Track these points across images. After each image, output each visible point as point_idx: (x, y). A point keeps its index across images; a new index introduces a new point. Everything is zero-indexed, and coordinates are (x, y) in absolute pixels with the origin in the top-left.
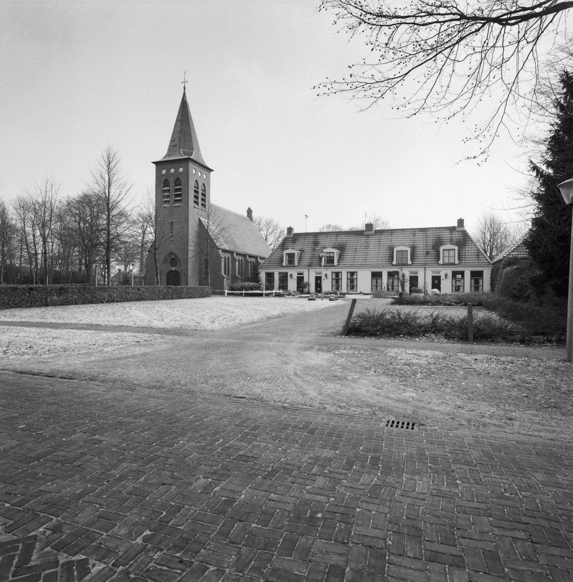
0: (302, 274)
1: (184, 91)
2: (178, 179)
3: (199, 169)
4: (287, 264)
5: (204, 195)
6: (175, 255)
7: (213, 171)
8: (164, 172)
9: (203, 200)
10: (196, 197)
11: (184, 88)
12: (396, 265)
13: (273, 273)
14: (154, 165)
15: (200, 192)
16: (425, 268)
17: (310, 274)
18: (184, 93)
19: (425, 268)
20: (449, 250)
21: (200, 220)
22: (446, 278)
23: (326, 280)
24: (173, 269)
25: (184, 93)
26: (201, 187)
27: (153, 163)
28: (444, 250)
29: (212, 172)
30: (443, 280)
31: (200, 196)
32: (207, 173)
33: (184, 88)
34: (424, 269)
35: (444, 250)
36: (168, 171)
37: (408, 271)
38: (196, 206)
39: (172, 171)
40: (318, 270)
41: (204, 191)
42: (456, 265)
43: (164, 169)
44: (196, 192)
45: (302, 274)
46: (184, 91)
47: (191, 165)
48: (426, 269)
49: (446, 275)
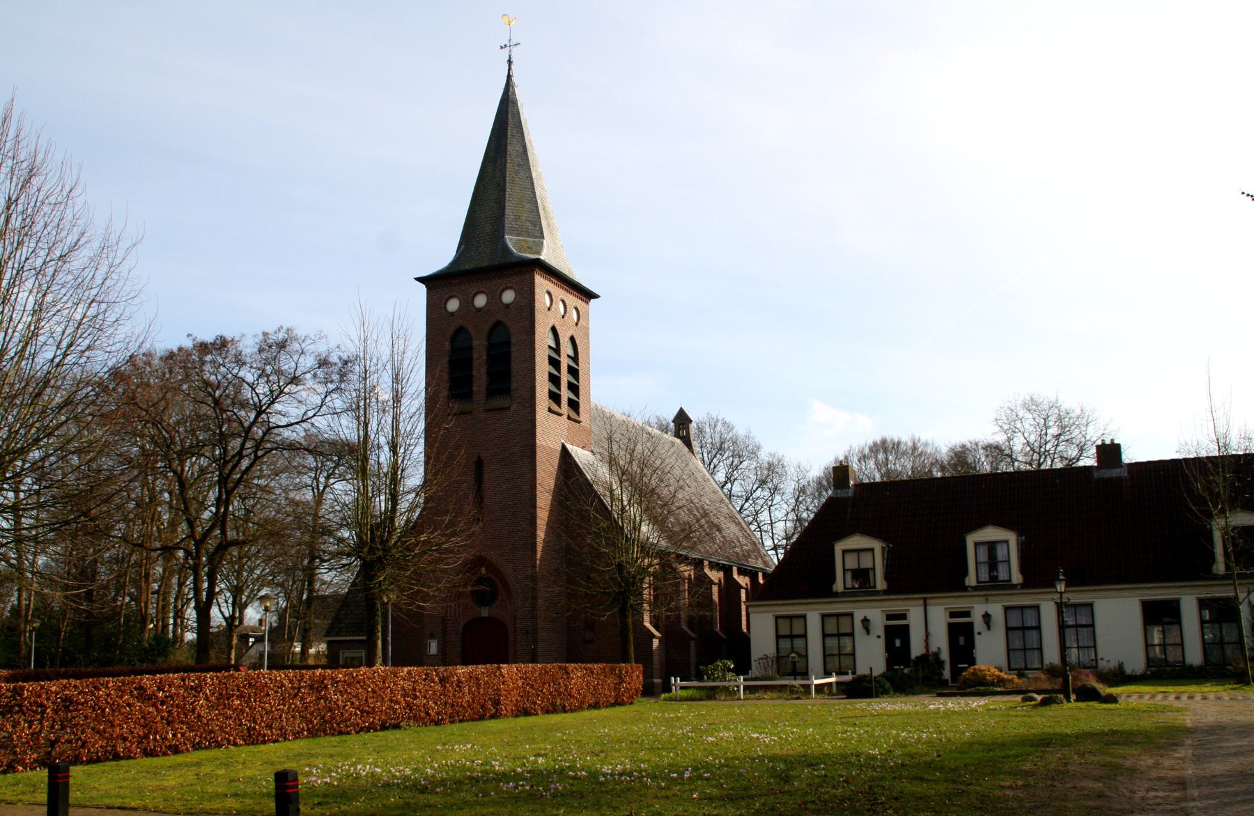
0: (904, 616)
1: (509, 69)
2: (498, 324)
3: (559, 293)
4: (849, 584)
5: (573, 372)
6: (491, 567)
7: (595, 296)
8: (453, 305)
9: (574, 388)
10: (554, 380)
11: (510, 62)
12: (843, 594)
13: (1177, 602)
14: (422, 289)
15: (565, 362)
16: (925, 599)
17: (1024, 616)
18: (509, 77)
19: (925, 599)
20: (858, 551)
21: (564, 448)
22: (989, 628)
23: (985, 634)
24: (485, 612)
25: (509, 77)
26: (567, 349)
27: (420, 280)
28: (844, 552)
29: (592, 300)
30: (979, 633)
31: (565, 377)
32: (580, 304)
33: (510, 62)
34: (921, 602)
35: (844, 552)
36: (494, 298)
37: (878, 611)
38: (555, 407)
39: (480, 301)
40: (959, 604)
41: (575, 358)
42: (1014, 587)
43: (451, 297)
44: (554, 363)
45: (903, 616)
46: (509, 69)
47: (542, 284)
48: (928, 601)
49: (987, 617)
